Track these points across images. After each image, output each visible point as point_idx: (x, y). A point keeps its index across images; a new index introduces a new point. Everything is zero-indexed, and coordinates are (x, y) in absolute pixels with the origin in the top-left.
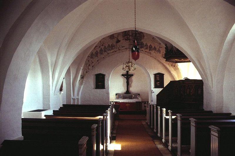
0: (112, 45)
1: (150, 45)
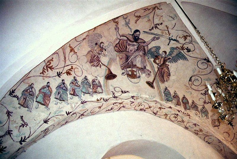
0: (93, 81)
1: (184, 97)
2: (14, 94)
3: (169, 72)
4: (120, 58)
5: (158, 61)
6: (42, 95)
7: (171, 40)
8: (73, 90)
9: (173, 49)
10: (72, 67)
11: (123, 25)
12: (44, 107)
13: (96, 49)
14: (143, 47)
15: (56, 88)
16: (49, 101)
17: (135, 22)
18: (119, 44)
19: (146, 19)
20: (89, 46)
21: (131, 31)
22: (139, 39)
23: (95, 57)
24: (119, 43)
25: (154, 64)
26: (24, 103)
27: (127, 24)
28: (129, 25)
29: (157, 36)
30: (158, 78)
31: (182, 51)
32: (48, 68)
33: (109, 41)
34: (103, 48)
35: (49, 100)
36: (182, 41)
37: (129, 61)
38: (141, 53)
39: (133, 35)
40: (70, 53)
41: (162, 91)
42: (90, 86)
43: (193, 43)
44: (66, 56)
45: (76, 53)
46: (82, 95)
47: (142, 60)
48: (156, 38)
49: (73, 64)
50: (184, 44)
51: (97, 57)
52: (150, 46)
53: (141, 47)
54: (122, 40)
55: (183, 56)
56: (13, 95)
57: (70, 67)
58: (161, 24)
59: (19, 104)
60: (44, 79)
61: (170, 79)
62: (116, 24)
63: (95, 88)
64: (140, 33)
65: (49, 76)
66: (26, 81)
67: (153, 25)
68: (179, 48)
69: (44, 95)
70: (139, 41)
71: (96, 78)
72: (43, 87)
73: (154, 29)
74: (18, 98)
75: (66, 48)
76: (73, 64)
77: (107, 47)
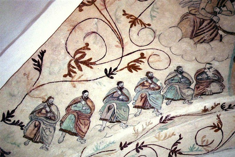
2: (12, 120)
6: (73, 117)
8: (142, 98)
10: (142, 54)
12: (76, 138)
15: (104, 100)
16: (87, 127)
20: (180, 4)
26: (35, 135)
32: (82, 65)
35: (88, 125)
40: (132, 29)
42: (190, 83)
44: (124, 36)
45: (149, 25)
46: (164, 105)
49: (142, 48)
51: (209, 21)
56: (10, 121)
57: (137, 56)
59: (25, 136)
60: (75, 87)
63: (201, 87)
65: (85, 79)
66: (36, 93)
69: (76, 116)
71: (208, 66)
72: (74, 100)
74: (22, 126)
75: (117, 19)
76: (142, 48)
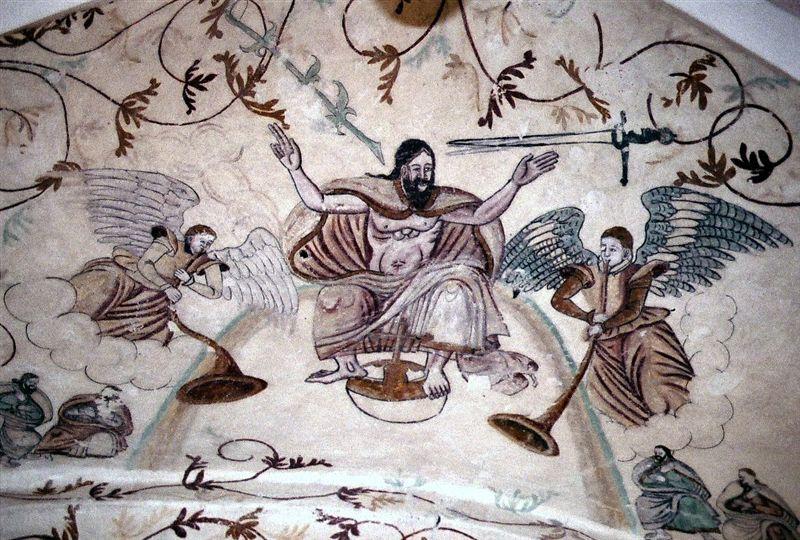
3: (681, 351)
4: (321, 306)
5: (589, 300)
7: (625, 143)
9: (660, 199)
11: (319, 127)
13: (152, 255)
14: (469, 228)
17: (382, 93)
18: (321, 240)
19: (436, 64)
21: (380, 158)
22: (439, 190)
23: (144, 296)
24: (318, 232)
25: (557, 318)
27: (339, 113)
28: (349, 117)
29: (539, 152)
30: (591, 395)
31: (721, 192)
33: (254, 222)
34: (211, 256)
36: (687, 119)
37: (385, 317)
38: (462, 268)
39: (395, 175)
41: (628, 473)
43: (759, 96)
47: (468, 307)
48: (538, 163)
50: (713, 134)
52: (512, 223)
53: (456, 235)
54: (334, 212)
55: (743, 219)
58: (529, 59)
61: (692, 396)
62: (272, 121)
64: (432, 155)
67: (487, 88)
68: (696, 180)
70: (441, 202)
73: (505, 106)
77: (235, 254)
